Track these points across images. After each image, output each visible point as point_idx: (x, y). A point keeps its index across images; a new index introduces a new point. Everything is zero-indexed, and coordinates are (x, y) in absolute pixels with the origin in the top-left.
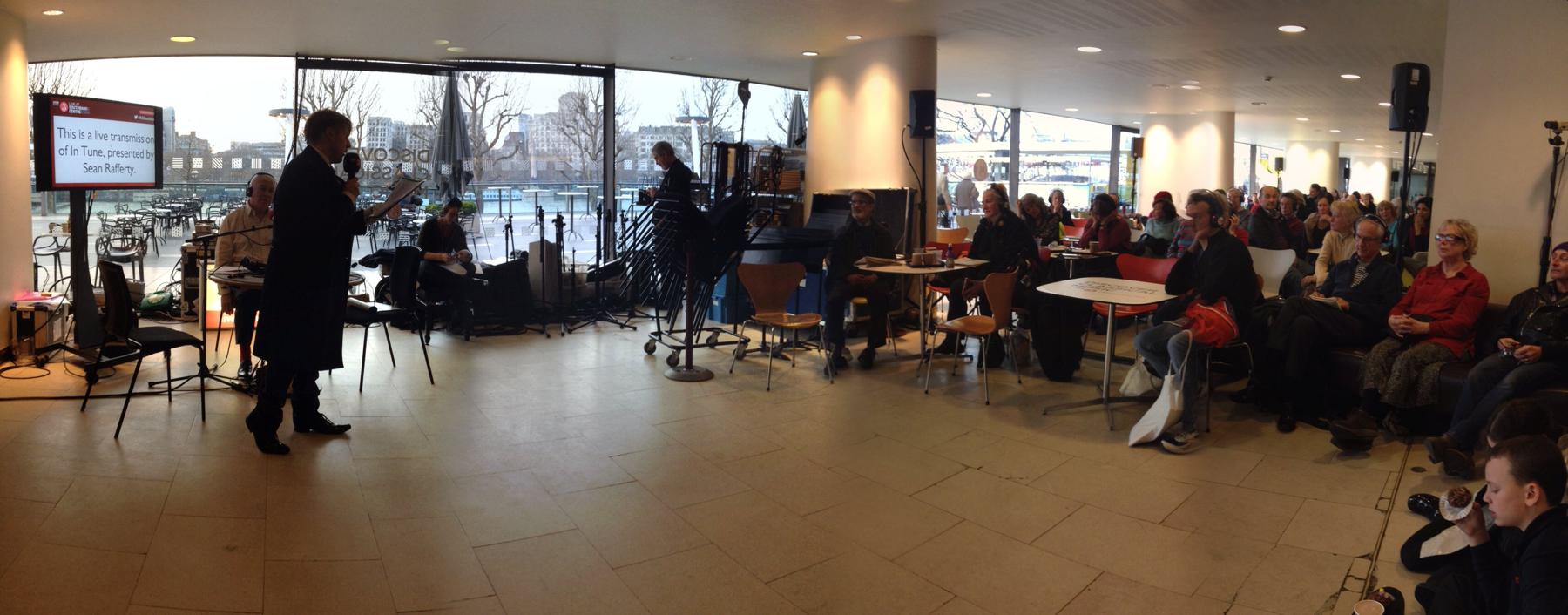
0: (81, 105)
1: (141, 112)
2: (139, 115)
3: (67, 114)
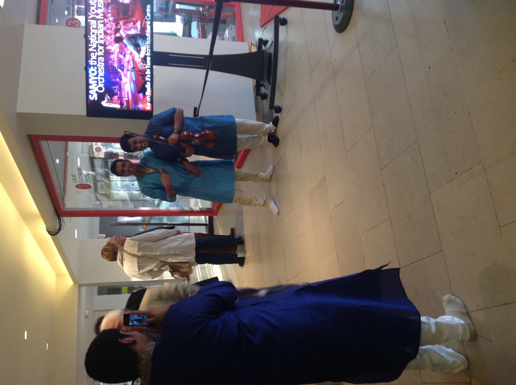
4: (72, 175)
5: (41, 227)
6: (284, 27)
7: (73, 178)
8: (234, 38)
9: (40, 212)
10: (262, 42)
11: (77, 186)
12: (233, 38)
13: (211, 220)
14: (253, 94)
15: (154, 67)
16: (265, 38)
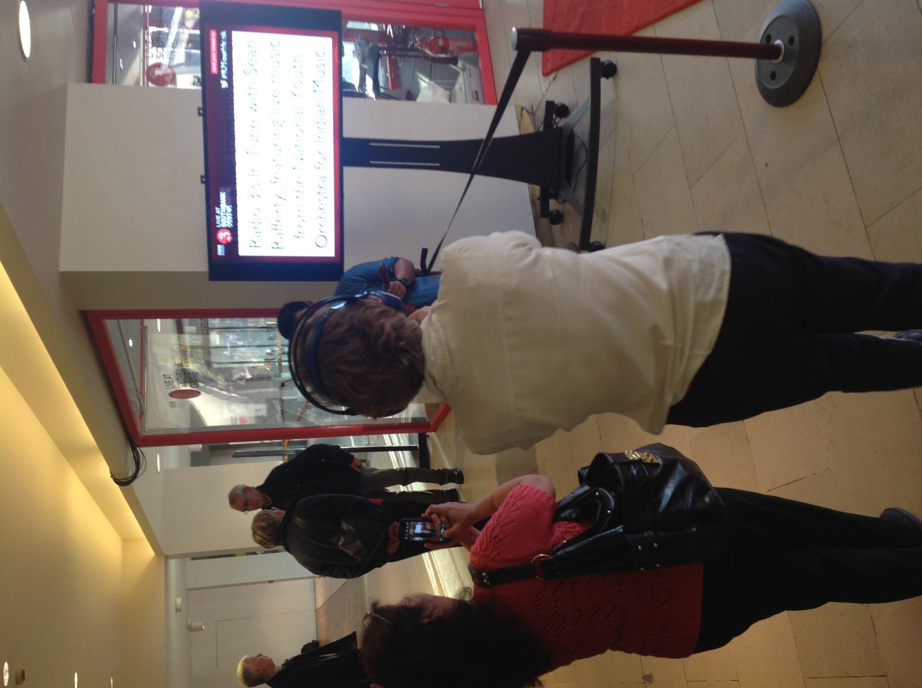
0: (219, 207)
1: (214, 70)
2: (218, 76)
3: (234, 230)
4: (164, 375)
5: (103, 470)
6: (611, 80)
7: (165, 382)
8: (476, 92)
9: (97, 444)
10: (555, 110)
11: (172, 394)
12: (474, 94)
13: (423, 439)
14: (531, 211)
15: (347, 170)
16: (559, 98)
